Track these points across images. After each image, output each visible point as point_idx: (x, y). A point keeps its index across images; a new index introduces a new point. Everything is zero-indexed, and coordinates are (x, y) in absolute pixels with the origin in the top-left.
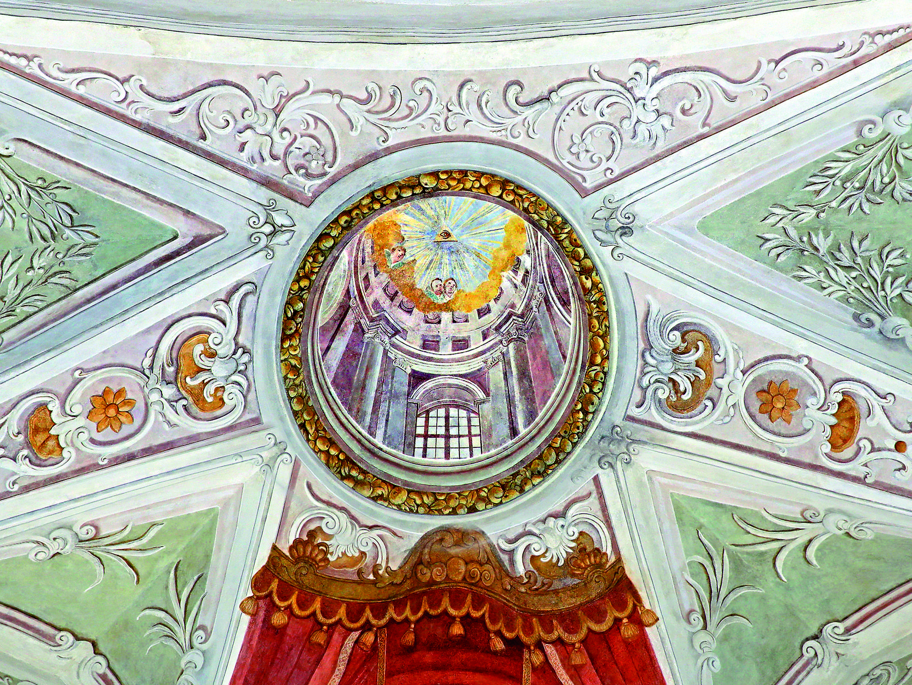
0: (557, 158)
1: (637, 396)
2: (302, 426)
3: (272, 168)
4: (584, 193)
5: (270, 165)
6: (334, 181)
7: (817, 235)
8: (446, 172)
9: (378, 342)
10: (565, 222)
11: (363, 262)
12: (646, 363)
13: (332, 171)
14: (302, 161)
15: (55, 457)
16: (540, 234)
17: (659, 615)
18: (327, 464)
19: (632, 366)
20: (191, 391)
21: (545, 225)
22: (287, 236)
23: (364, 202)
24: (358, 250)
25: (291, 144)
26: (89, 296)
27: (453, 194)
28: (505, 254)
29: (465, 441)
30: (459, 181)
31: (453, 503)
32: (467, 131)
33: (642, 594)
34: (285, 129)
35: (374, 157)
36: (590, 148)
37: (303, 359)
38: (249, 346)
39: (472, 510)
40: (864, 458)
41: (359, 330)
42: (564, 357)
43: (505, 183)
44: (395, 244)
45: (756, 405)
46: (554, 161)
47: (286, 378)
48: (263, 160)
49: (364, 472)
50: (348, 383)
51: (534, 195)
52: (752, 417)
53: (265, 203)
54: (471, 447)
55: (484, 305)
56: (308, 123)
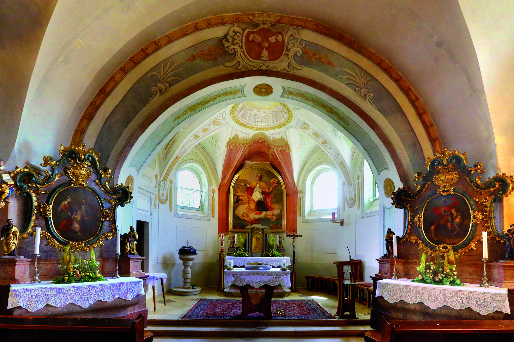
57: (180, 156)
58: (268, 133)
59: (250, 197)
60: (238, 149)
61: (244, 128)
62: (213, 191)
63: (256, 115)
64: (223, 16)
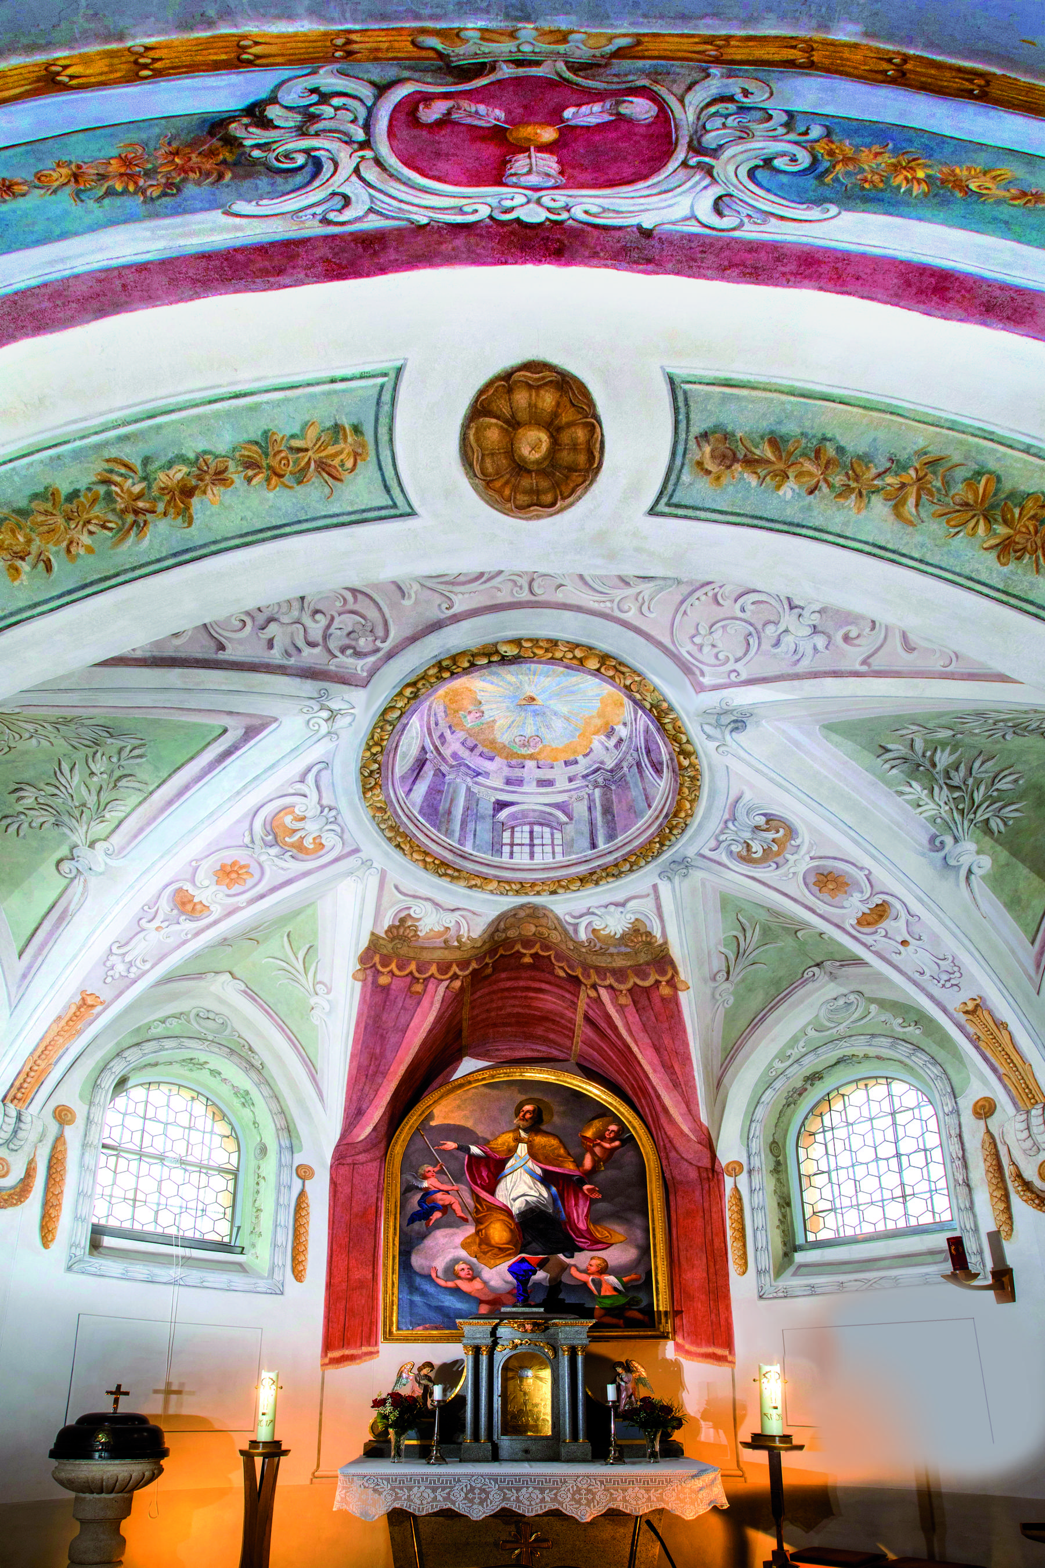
0: (673, 643)
1: (713, 843)
2: (398, 846)
3: (311, 656)
4: (700, 688)
5: (310, 654)
6: (390, 655)
7: (943, 751)
8: (530, 640)
9: (461, 785)
10: (671, 709)
11: (437, 724)
12: (727, 827)
13: (386, 646)
14: (347, 641)
15: (206, 913)
16: (640, 712)
17: (690, 984)
18: (425, 868)
19: (713, 825)
20: (292, 845)
21: (648, 706)
22: (349, 719)
23: (431, 672)
24: (429, 716)
25: (328, 627)
26: (168, 798)
27: (540, 663)
28: (599, 722)
29: (548, 849)
30: (547, 650)
31: (537, 888)
32: (560, 597)
33: (680, 969)
34: (317, 612)
35: (436, 626)
36: (719, 644)
37: (388, 802)
38: (333, 804)
39: (554, 893)
40: (876, 937)
41: (440, 774)
42: (650, 806)
43: (604, 658)
44: (471, 708)
45: (812, 879)
46: (673, 648)
47: (374, 817)
48: (299, 650)
49: (458, 871)
50: (435, 810)
51: (639, 675)
52: (806, 884)
53: (316, 695)
54: (553, 853)
55: (572, 758)
56: (345, 599)
57: (106, 995)
58: (563, 906)
59: (484, 1195)
60: (418, 988)
61: (444, 882)
62: (304, 1173)
63: (501, 805)
64: (244, 37)
